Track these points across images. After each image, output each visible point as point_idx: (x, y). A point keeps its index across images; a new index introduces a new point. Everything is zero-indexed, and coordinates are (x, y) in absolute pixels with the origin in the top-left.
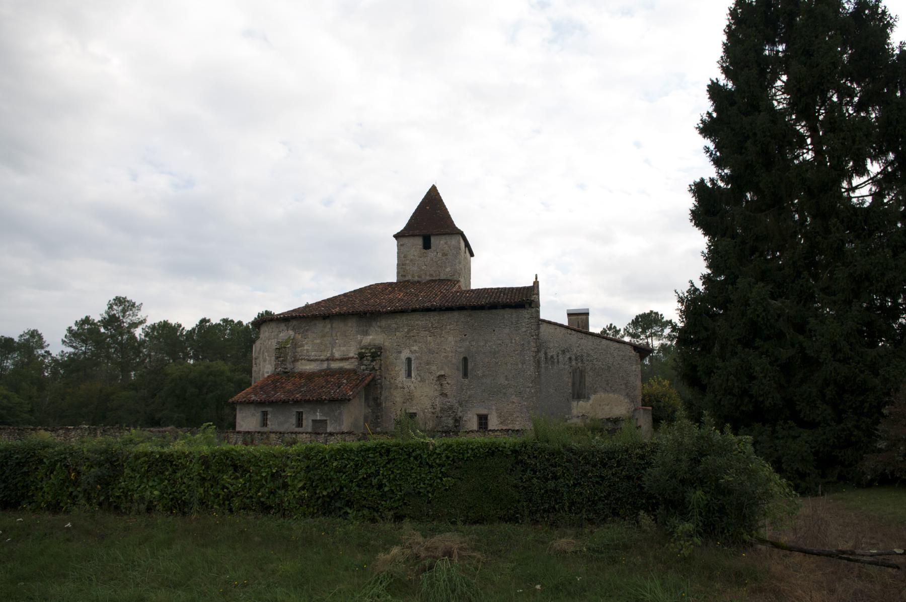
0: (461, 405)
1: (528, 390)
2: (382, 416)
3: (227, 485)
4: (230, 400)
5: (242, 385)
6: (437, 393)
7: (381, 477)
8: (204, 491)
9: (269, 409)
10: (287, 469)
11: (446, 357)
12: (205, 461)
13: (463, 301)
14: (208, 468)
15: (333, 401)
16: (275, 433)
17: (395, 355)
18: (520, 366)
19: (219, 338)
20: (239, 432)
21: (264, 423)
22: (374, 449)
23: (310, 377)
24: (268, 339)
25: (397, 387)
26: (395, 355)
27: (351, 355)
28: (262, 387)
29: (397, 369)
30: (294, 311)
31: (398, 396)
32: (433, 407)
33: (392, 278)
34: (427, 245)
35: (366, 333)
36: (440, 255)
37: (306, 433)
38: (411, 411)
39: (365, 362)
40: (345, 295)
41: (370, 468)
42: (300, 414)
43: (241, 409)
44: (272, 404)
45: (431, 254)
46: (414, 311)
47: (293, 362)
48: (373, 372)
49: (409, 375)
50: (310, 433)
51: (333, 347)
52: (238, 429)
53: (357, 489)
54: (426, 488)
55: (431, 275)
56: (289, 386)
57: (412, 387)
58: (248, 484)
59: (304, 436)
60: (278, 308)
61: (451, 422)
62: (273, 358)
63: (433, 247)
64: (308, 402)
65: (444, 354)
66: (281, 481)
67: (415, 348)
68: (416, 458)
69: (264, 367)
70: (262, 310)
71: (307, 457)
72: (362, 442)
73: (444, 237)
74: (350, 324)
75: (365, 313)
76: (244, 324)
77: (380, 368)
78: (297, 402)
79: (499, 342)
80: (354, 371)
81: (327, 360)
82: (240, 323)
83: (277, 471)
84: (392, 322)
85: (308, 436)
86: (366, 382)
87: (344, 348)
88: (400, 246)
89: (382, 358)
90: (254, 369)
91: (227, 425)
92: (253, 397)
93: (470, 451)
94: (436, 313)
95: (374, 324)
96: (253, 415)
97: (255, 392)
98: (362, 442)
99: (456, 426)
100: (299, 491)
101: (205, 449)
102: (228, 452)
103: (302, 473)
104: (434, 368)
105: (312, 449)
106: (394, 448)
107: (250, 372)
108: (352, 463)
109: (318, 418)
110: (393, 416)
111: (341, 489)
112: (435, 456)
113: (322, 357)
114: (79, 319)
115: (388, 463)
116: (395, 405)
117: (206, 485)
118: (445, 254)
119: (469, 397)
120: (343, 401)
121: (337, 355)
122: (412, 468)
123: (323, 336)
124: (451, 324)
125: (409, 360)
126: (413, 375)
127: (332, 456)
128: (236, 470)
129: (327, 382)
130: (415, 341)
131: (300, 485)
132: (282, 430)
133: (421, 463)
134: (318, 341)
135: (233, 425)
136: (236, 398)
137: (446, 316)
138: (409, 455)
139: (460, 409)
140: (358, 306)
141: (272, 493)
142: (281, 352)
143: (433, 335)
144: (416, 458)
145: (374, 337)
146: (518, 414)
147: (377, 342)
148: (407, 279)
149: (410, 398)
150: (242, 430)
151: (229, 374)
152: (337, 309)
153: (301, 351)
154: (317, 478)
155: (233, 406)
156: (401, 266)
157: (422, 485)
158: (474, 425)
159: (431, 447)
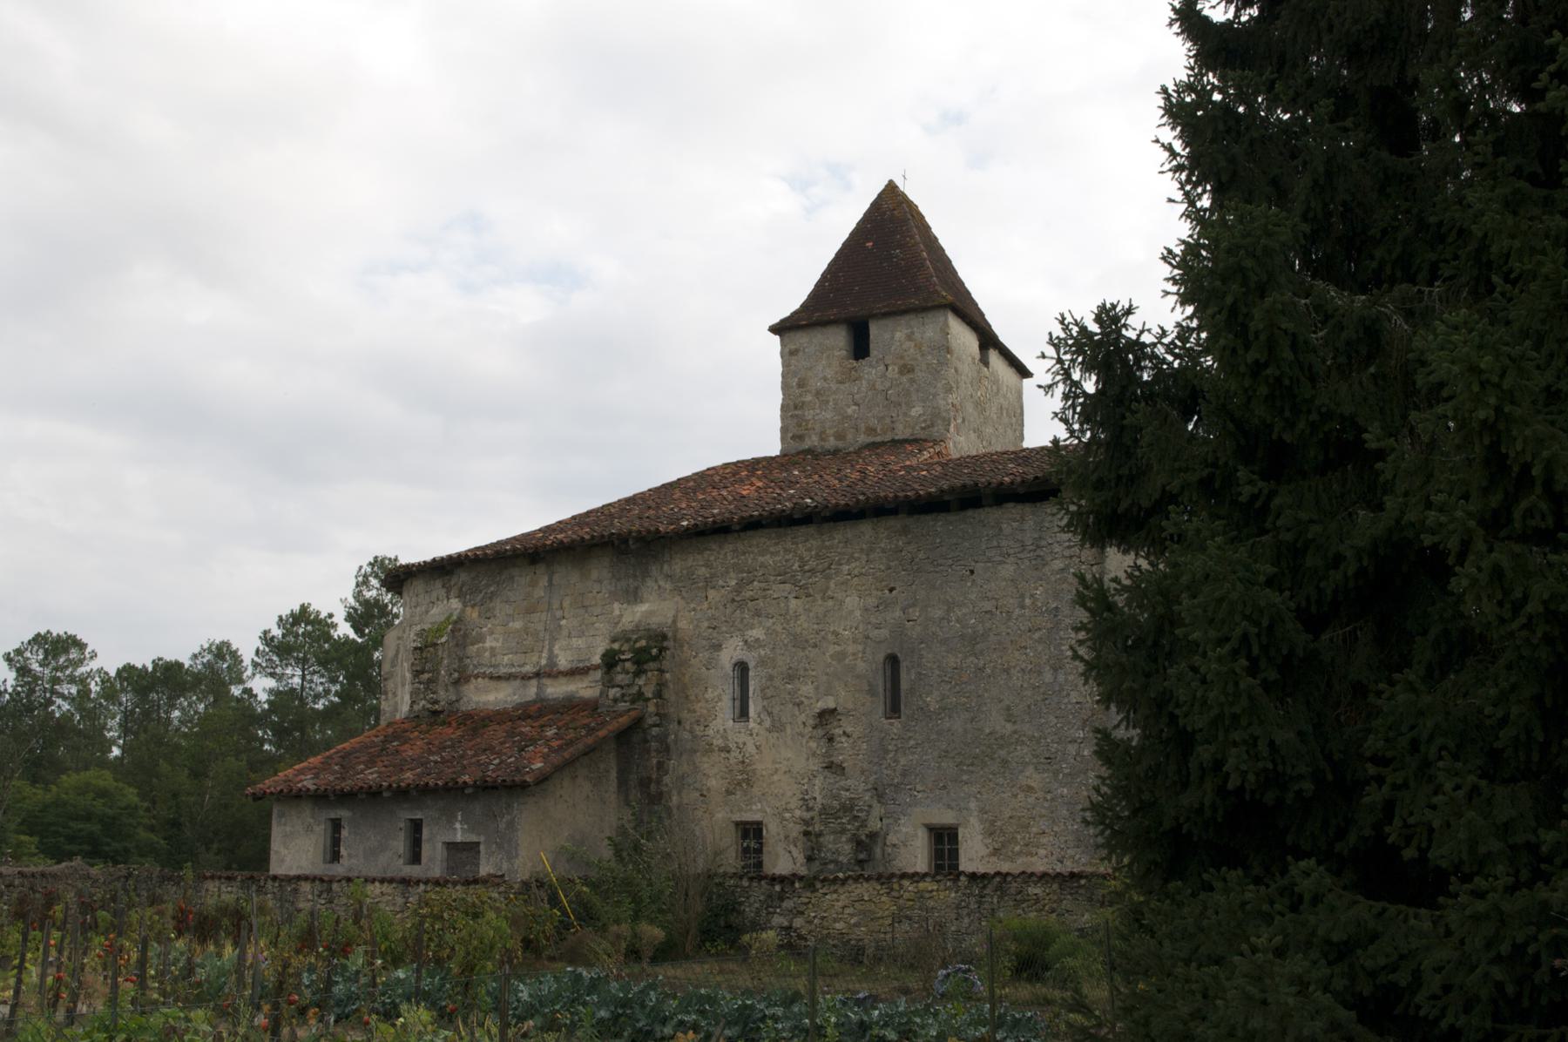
0: (880, 796)
1: (1072, 749)
6: (815, 765)
9: (343, 813)
18: (1048, 676)
25: (709, 749)
29: (709, 695)
32: (806, 804)
33: (771, 446)
34: (860, 348)
35: (634, 596)
36: (893, 371)
43: (281, 815)
44: (345, 797)
45: (869, 370)
46: (752, 525)
47: (456, 683)
49: (744, 714)
51: (553, 640)
52: (276, 868)
55: (871, 431)
57: (751, 749)
63: (874, 352)
65: (833, 649)
67: (757, 633)
73: (903, 320)
74: (595, 574)
77: (659, 695)
78: (403, 794)
79: (988, 606)
80: (591, 706)
81: (537, 675)
85: (386, 888)
88: (788, 355)
89: (666, 664)
94: (811, 529)
96: (309, 829)
104: (807, 689)
109: (459, 838)
113: (528, 669)
114: (285, 612)
118: (906, 369)
119: (904, 774)
123: (530, 610)
124: (851, 559)
125: (742, 668)
130: (757, 614)
134: (517, 625)
135: (262, 858)
139: (878, 809)
143: (804, 592)
145: (654, 607)
146: (1043, 824)
147: (654, 621)
148: (806, 445)
149: (743, 780)
153: (479, 654)
156: (792, 411)
158: (916, 855)
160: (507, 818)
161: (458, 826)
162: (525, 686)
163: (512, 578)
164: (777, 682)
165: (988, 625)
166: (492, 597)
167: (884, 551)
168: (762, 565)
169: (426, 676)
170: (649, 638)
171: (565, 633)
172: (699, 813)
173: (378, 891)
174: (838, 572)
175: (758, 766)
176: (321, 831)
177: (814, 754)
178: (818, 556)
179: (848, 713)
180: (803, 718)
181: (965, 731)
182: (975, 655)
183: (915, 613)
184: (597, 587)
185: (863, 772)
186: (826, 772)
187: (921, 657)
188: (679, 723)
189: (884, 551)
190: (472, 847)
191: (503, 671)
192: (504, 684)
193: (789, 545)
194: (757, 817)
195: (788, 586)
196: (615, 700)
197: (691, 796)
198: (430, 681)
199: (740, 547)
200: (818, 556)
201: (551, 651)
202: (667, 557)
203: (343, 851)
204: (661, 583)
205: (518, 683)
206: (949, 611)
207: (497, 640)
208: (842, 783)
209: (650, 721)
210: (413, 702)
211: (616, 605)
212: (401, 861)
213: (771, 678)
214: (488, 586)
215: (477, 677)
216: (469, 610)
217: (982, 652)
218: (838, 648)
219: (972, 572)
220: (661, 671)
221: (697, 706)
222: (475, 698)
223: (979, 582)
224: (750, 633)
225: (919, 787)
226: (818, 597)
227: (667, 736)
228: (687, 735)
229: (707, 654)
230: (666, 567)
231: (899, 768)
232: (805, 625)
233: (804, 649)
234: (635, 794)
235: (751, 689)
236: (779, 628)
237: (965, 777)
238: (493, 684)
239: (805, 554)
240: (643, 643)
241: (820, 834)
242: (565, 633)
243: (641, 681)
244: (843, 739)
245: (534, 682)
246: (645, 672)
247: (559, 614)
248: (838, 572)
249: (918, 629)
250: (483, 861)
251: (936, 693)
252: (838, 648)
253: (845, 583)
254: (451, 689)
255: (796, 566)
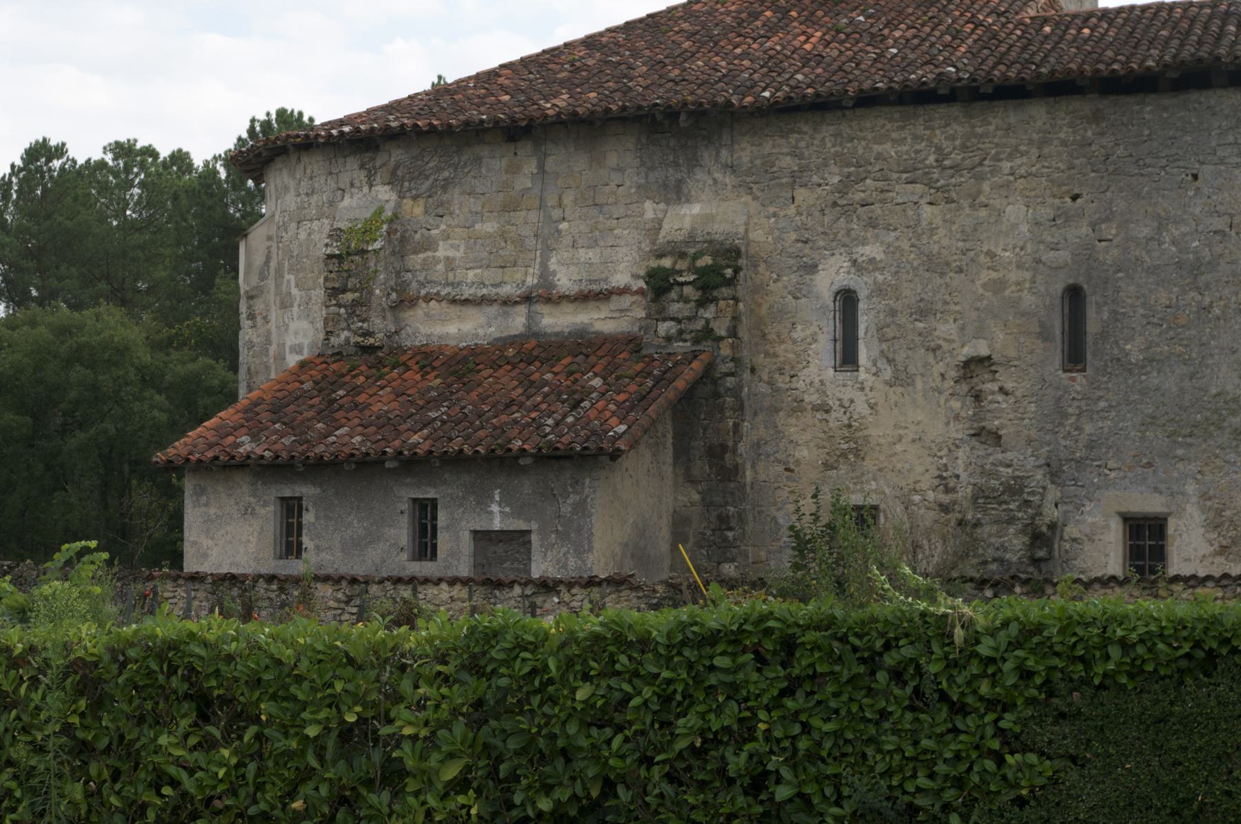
2: (741, 518)
3: (172, 770)
4: (159, 457)
5: (196, 401)
6: (957, 431)
7: (759, 746)
8: (89, 795)
9: (306, 491)
10: (401, 712)
11: (998, 286)
12: (86, 679)
13: (1072, 61)
14: (98, 705)
15: (553, 458)
16: (335, 580)
17: (790, 279)
19: (103, 219)
20: (196, 578)
21: (291, 546)
22: (733, 638)
23: (462, 365)
24: (295, 225)
25: (798, 407)
26: (790, 279)
27: (620, 279)
28: (281, 405)
29: (798, 334)
30: (393, 107)
31: (804, 444)
32: (945, 483)
35: (676, 193)
37: (453, 582)
38: (856, 499)
39: (675, 308)
40: (591, 42)
41: (719, 711)
42: (425, 513)
43: (200, 491)
46: (869, 100)
47: (397, 307)
48: (706, 345)
49: (848, 358)
50: (465, 582)
51: (548, 250)
52: (191, 565)
53: (668, 789)
54: (938, 793)
56: (383, 403)
58: (252, 768)
59: (444, 591)
60: (324, 106)
61: (1015, 544)
62: (319, 294)
64: (457, 461)
65: (986, 275)
66: (377, 757)
68: (897, 675)
69: (285, 329)
70: (264, 107)
71: (475, 667)
72: (684, 613)
74: (612, 160)
75: (672, 114)
76: (198, 162)
77: (733, 333)
78: (412, 464)
79: (1219, 223)
80: (632, 343)
81: (527, 299)
82: (180, 158)
83: (362, 720)
84: (780, 150)
85: (459, 592)
86: (680, 384)
87: (592, 255)
89: (741, 291)
90: (247, 334)
91: (149, 551)
92: (247, 445)
93: (1115, 652)
94: (955, 110)
95: (707, 156)
96: (248, 511)
97: (252, 423)
98: (684, 613)
99: (1035, 561)
100: (444, 797)
101: (88, 637)
102: (173, 646)
103: (459, 728)
104: (946, 329)
105: (493, 635)
106: (811, 636)
107: (225, 348)
108: (647, 692)
109: (497, 525)
110: (784, 518)
111: (609, 786)
112: (974, 668)
113: (507, 290)
115: (788, 692)
116: (793, 476)
117: (93, 769)
119: (1090, 446)
120: (589, 458)
121: (565, 281)
122: (884, 714)
123: (510, 207)
124: (1015, 152)
125: (847, 300)
126: (863, 357)
127: (570, 663)
128: (204, 717)
129: (530, 385)
130: (872, 224)
131: (451, 772)
132: (359, 570)
133: (917, 692)
135: (170, 553)
136: (178, 448)
137: (996, 123)
138: (872, 661)
139: (1053, 493)
140: (645, 87)
141: (343, 801)
142: (346, 269)
143: (942, 196)
144: (897, 675)
145: (709, 208)
147: (719, 229)
149: (850, 448)
150: (206, 568)
151: (144, 356)
152: (563, 101)
153: (426, 266)
154: (512, 744)
155: (169, 482)
157: (922, 781)
158: (1107, 553)
159: (959, 634)
160: (573, 498)
161: (495, 508)
162: (506, 314)
163: (478, 160)
164: (902, 319)
165: (1218, 249)
166: (446, 185)
167: (1064, 143)
168: (879, 157)
169: (349, 296)
170: (715, 254)
171: (567, 240)
172: (784, 494)
173: (445, 596)
174: (995, 171)
175: (872, 432)
176: (268, 515)
177: (957, 417)
178: (964, 147)
179: (1007, 363)
180: (941, 368)
181: (1182, 390)
182: (1198, 289)
183: (1110, 230)
184: (616, 178)
185: (1029, 442)
186: (974, 442)
187: (1118, 290)
188: (753, 370)
189: (1064, 143)
190: (520, 539)
191: (467, 292)
192: (471, 311)
193: (920, 130)
194: (873, 500)
195: (919, 188)
196: (669, 339)
197: (770, 471)
198: (355, 304)
199: (845, 129)
200: (964, 147)
201: (544, 265)
202: (726, 138)
203: (306, 541)
204: (718, 176)
205: (493, 310)
206: (1160, 228)
207: (457, 248)
208: (1000, 456)
209: (724, 368)
210: (329, 333)
211: (648, 205)
212: (405, 556)
213: (893, 313)
214: (439, 170)
215: (428, 299)
216: (408, 203)
217: (1207, 286)
218: (993, 275)
219: (1195, 177)
220: (736, 300)
221: (780, 349)
222: (424, 329)
223: (1206, 190)
224: (860, 249)
225: (1111, 464)
226: (965, 203)
227: (741, 388)
228: (763, 388)
229: (794, 278)
230: (724, 153)
231: (1083, 438)
232: (945, 242)
233: (942, 274)
234: (701, 467)
235: (862, 328)
236: (905, 245)
237: (1180, 452)
238: (454, 310)
239: (945, 144)
240: (706, 261)
241: (977, 524)
242: (567, 240)
243: (709, 312)
244: (1000, 398)
245: (522, 309)
246: (715, 300)
247: (557, 213)
248: (995, 171)
249: (1115, 252)
250: (536, 555)
251: (1139, 340)
252: (993, 275)
253: (1007, 185)
254: (388, 314)
255: (931, 160)
